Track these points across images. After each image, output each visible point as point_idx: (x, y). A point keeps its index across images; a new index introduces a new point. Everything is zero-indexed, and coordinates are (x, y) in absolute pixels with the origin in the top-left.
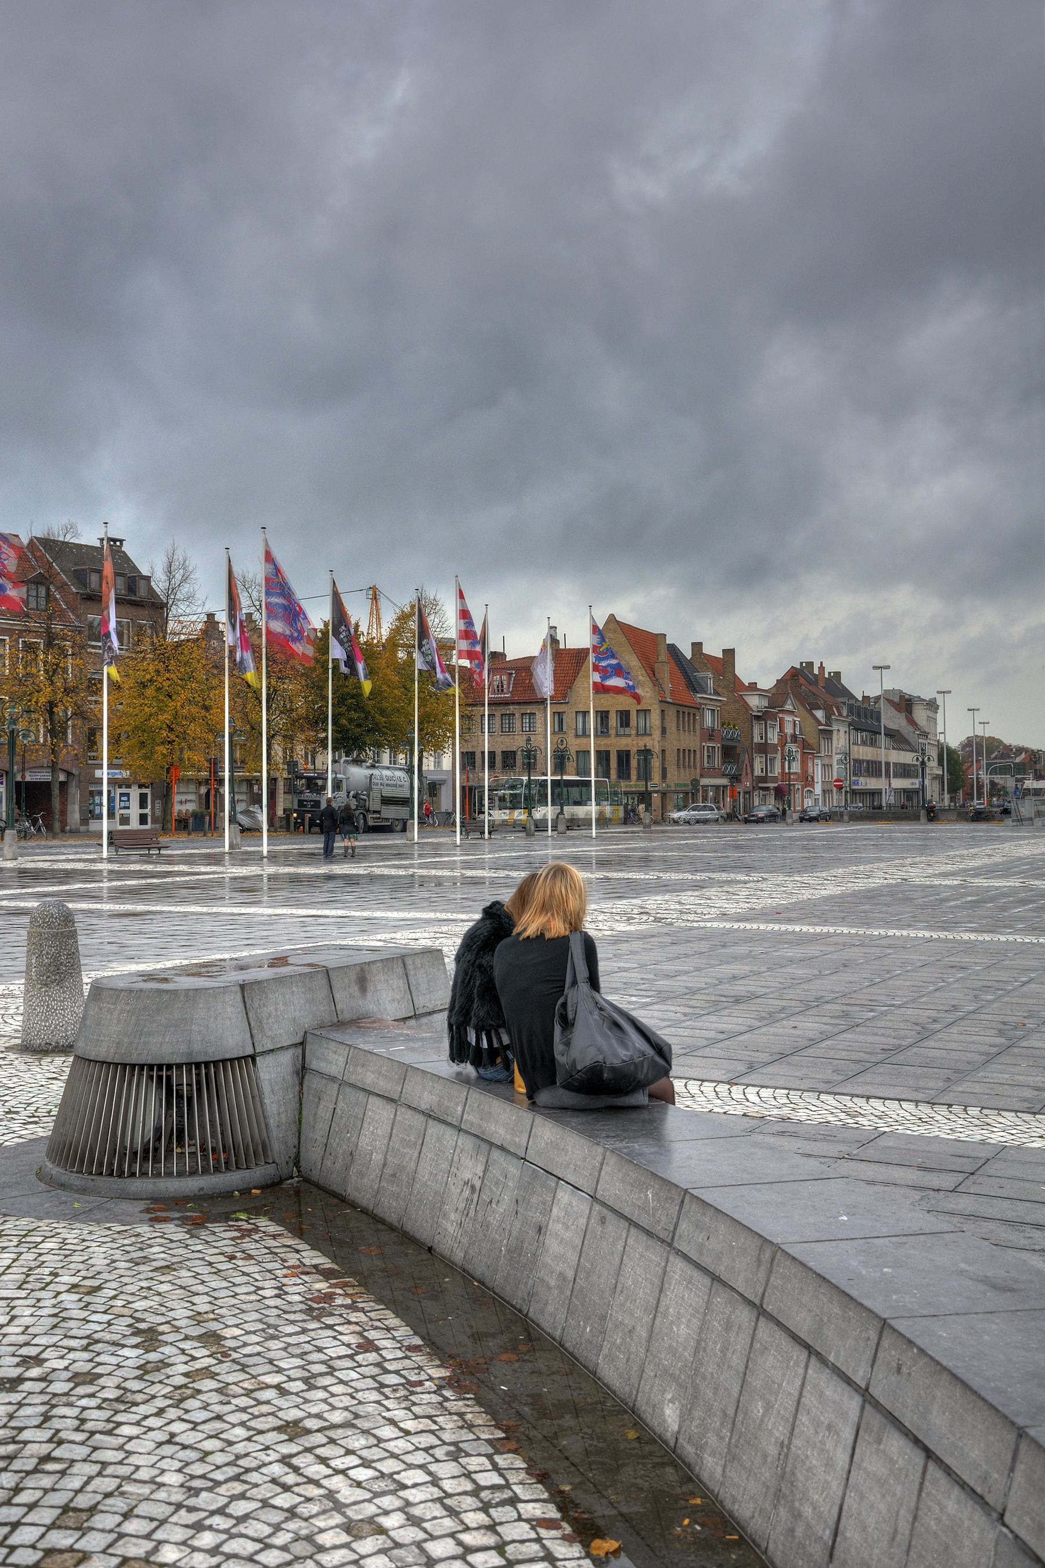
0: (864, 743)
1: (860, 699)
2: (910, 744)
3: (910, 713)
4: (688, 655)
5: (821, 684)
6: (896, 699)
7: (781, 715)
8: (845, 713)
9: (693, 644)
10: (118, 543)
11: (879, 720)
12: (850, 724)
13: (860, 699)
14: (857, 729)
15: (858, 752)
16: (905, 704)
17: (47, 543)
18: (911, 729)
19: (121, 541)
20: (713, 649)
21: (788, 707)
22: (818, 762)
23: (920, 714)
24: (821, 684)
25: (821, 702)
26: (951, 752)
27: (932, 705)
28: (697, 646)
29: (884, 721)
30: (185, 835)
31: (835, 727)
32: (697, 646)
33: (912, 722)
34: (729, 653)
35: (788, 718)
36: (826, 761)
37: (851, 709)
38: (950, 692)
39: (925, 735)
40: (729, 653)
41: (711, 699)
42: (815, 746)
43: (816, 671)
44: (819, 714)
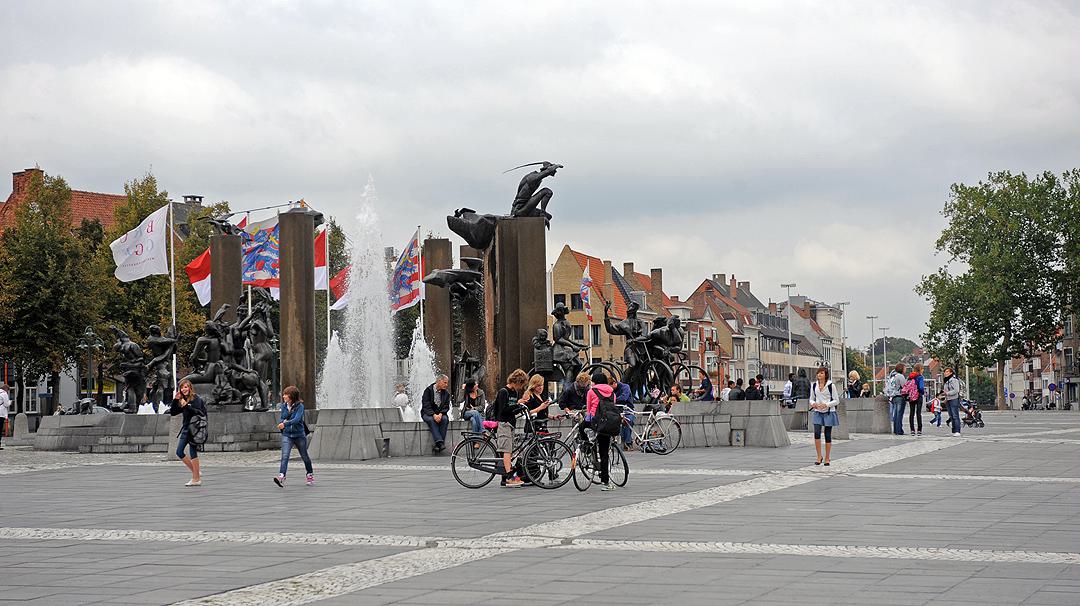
0: (772, 349)
1: (767, 306)
2: (814, 349)
3: (815, 319)
4: (621, 271)
5: (733, 295)
6: (802, 306)
7: (700, 326)
8: (755, 322)
9: (660, 270)
10: (198, 200)
11: (785, 326)
12: (760, 332)
13: (767, 306)
14: (765, 337)
15: (767, 357)
16: (811, 311)
17: (489, 217)
18: (815, 334)
19: (200, 198)
20: (643, 268)
21: (707, 318)
22: (732, 367)
23: (824, 320)
24: (733, 295)
25: (733, 312)
26: (489, 225)
27: (836, 311)
28: (628, 266)
29: (791, 329)
30: (160, 465)
31: (746, 335)
32: (628, 266)
33: (817, 328)
34: (657, 272)
35: (707, 328)
36: (739, 366)
37: (760, 317)
38: (794, 285)
39: (829, 340)
40: (657, 272)
41: (645, 314)
42: (729, 353)
43: (728, 283)
44: (732, 323)
